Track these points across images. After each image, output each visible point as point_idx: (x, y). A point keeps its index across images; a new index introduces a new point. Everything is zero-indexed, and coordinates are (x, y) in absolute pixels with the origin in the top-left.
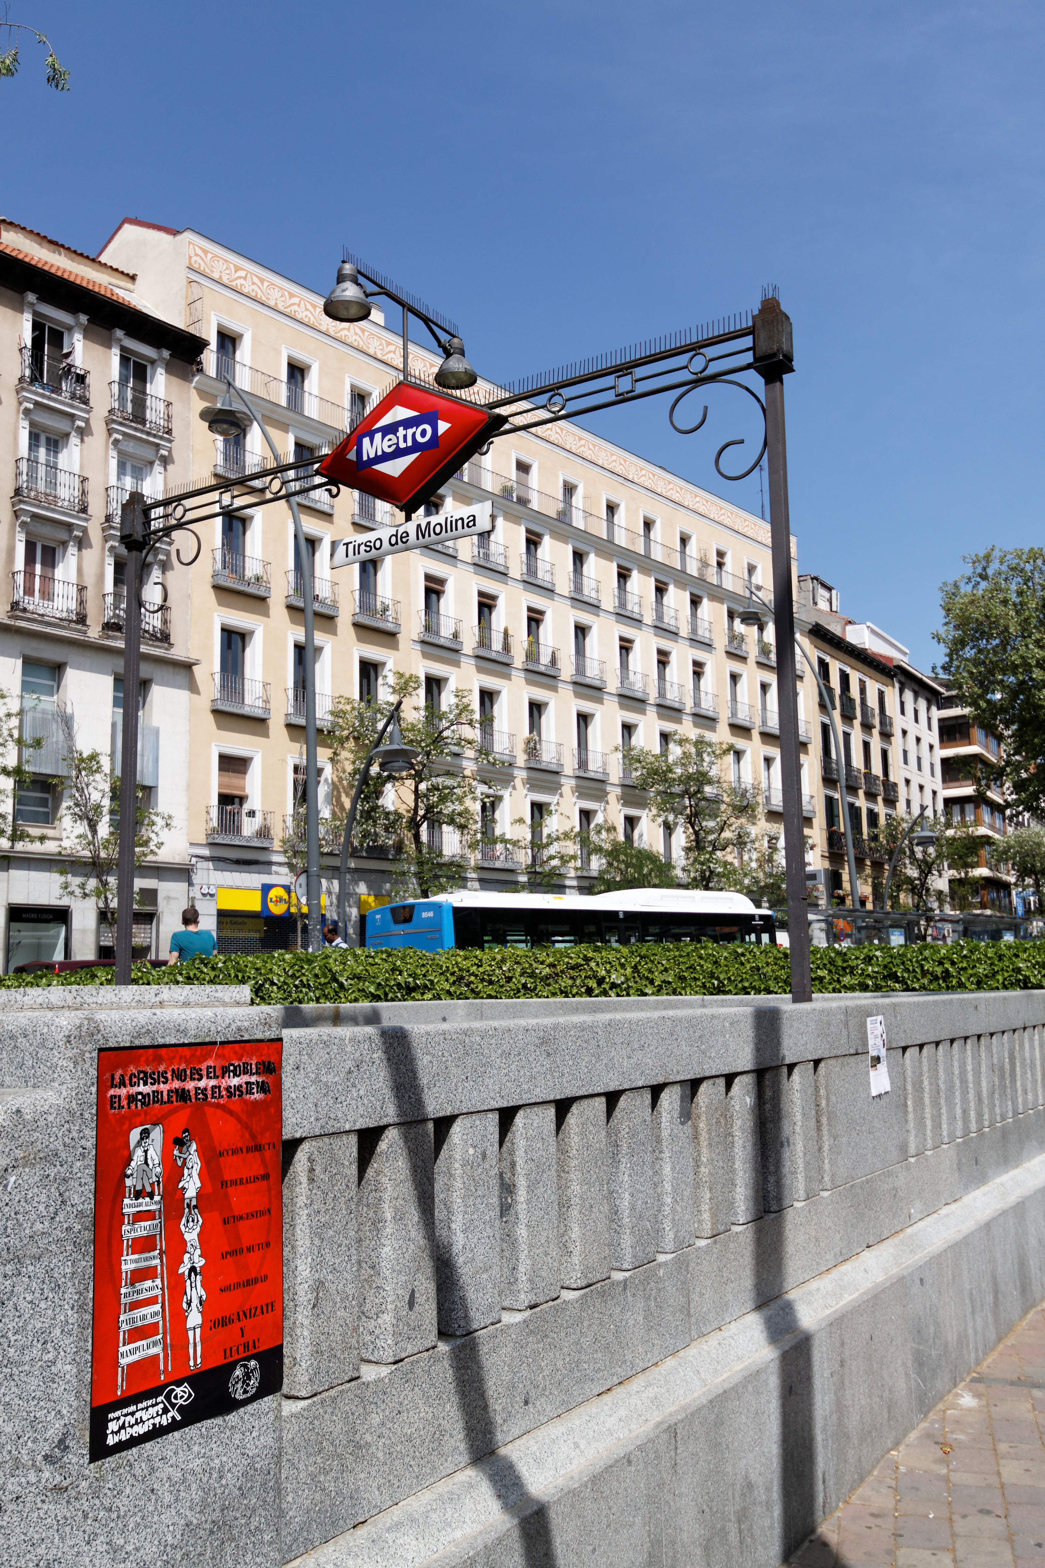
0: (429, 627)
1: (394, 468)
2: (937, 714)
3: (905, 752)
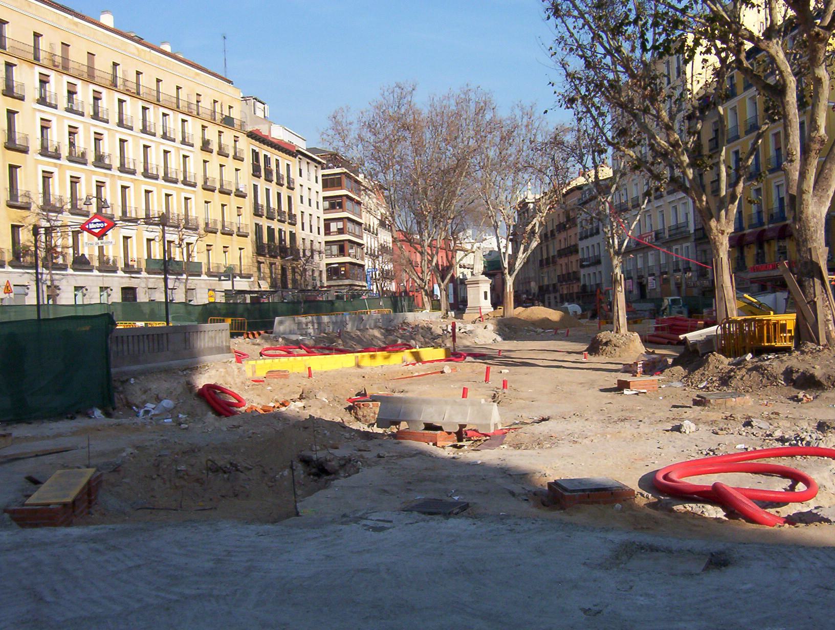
0: (70, 153)
1: (96, 231)
2: (321, 172)
3: (302, 197)
